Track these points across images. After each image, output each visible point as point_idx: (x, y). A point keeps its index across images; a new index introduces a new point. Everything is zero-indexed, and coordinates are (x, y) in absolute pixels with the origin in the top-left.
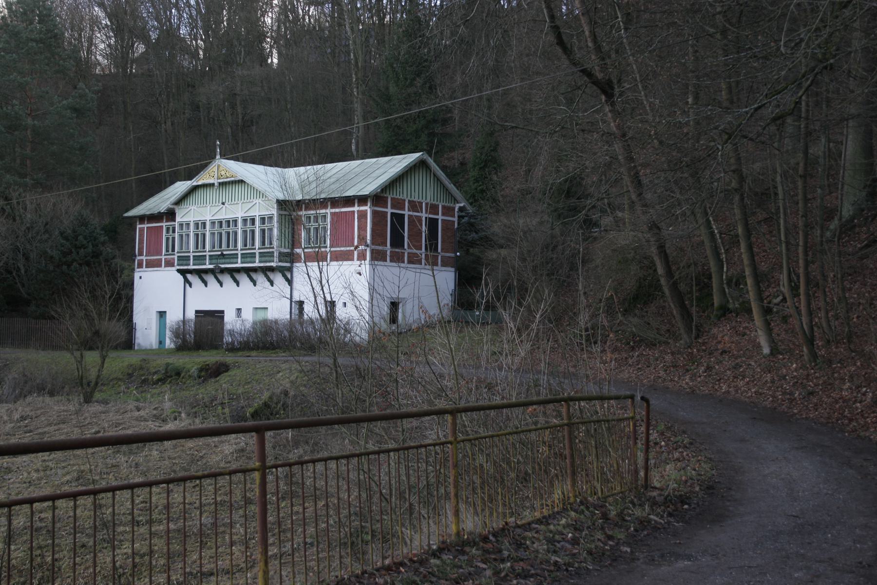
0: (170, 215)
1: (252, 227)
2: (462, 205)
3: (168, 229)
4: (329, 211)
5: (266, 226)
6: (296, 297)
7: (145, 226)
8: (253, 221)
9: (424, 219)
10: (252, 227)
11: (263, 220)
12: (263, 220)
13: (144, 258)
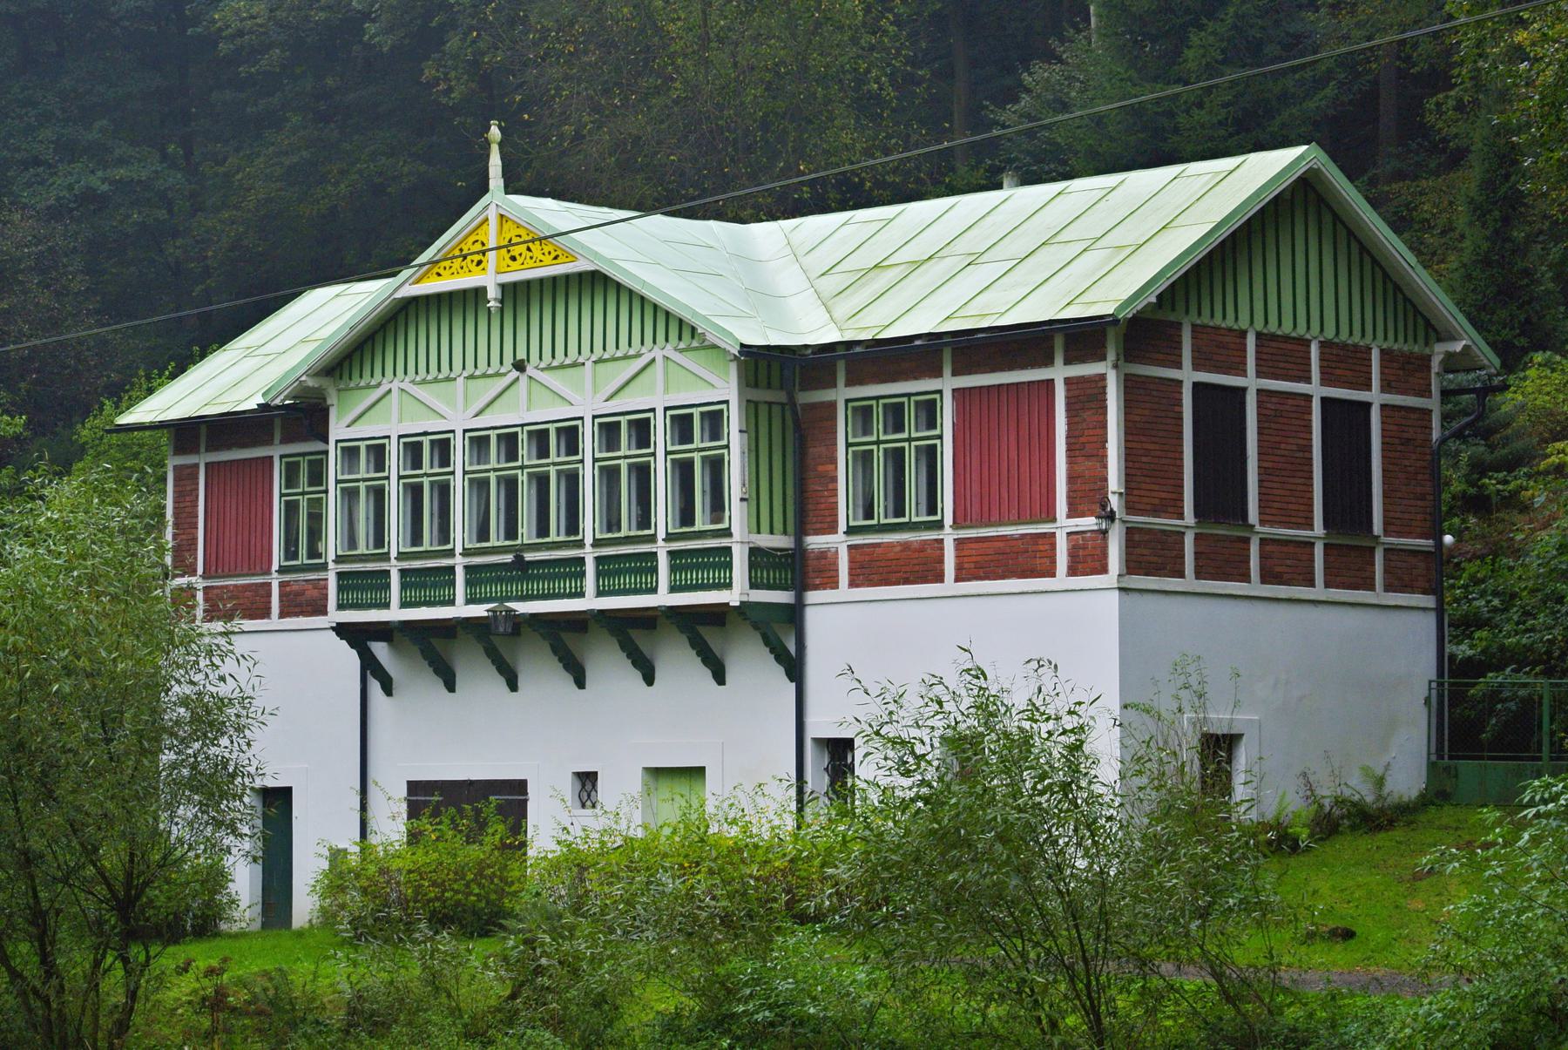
4: (948, 384)
6: (821, 725)
7: (202, 460)
12: (682, 426)
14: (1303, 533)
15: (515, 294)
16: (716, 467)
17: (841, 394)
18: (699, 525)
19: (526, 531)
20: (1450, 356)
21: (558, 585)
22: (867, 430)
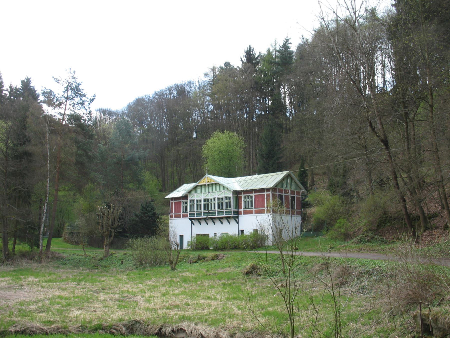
0: (185, 197)
1: (214, 202)
2: (303, 191)
3: (183, 203)
4: (254, 194)
5: (228, 201)
6: (240, 229)
7: (174, 202)
8: (222, 199)
9: (290, 197)
10: (222, 201)
11: (226, 198)
12: (226, 198)
13: (173, 214)
14: (289, 209)
15: (208, 185)
16: (230, 203)
17: (243, 195)
18: (228, 208)
19: (209, 209)
20: (302, 192)
21: (213, 214)
22: (245, 199)
